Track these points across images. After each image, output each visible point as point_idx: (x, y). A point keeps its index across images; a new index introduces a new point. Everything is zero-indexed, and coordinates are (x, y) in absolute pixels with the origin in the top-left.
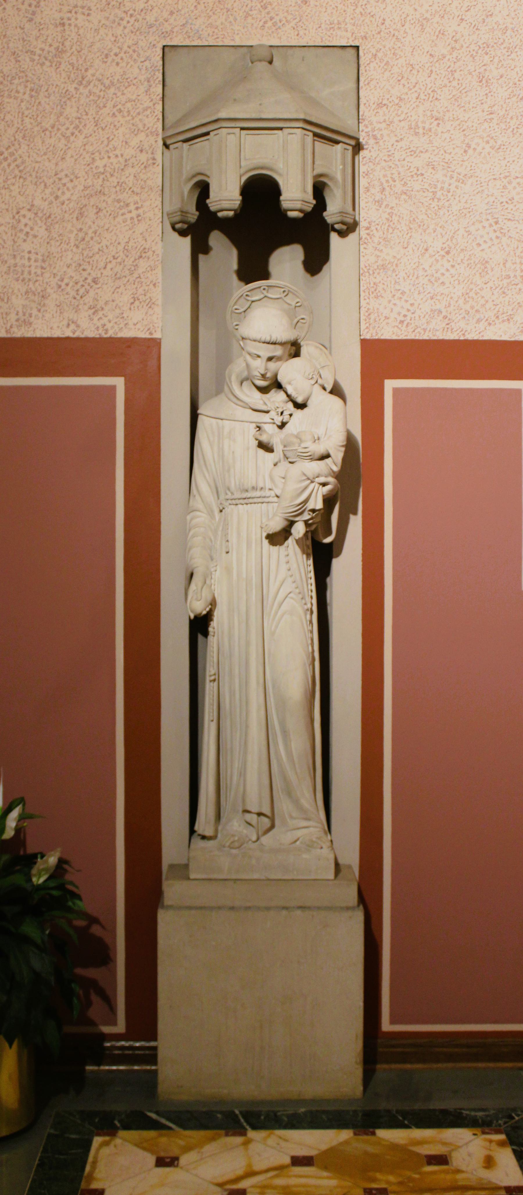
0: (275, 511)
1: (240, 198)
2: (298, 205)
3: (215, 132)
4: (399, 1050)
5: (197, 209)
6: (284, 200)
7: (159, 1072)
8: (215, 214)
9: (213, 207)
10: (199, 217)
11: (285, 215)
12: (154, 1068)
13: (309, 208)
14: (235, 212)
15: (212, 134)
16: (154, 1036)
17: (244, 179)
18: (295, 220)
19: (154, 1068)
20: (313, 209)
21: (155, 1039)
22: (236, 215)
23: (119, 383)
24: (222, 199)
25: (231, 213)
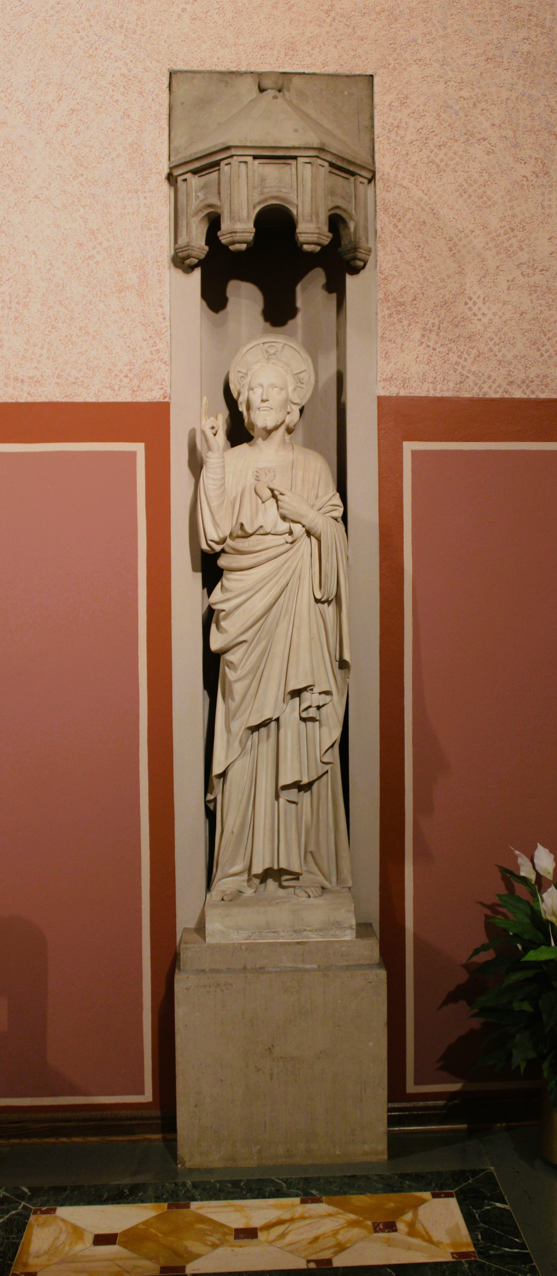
0: (250, 738)
1: (254, 230)
2: (314, 238)
3: (226, 161)
4: (74, 1124)
5: (207, 244)
6: (300, 233)
7: (386, 1125)
8: (225, 247)
9: (224, 240)
10: (208, 255)
11: (301, 248)
12: (390, 1114)
13: (326, 241)
14: (247, 245)
15: (223, 164)
16: (390, 1135)
17: (258, 209)
18: (311, 254)
19: (390, 1114)
20: (330, 243)
21: (388, 1131)
22: (248, 249)
23: (139, 448)
24: (231, 144)
25: (244, 247)
